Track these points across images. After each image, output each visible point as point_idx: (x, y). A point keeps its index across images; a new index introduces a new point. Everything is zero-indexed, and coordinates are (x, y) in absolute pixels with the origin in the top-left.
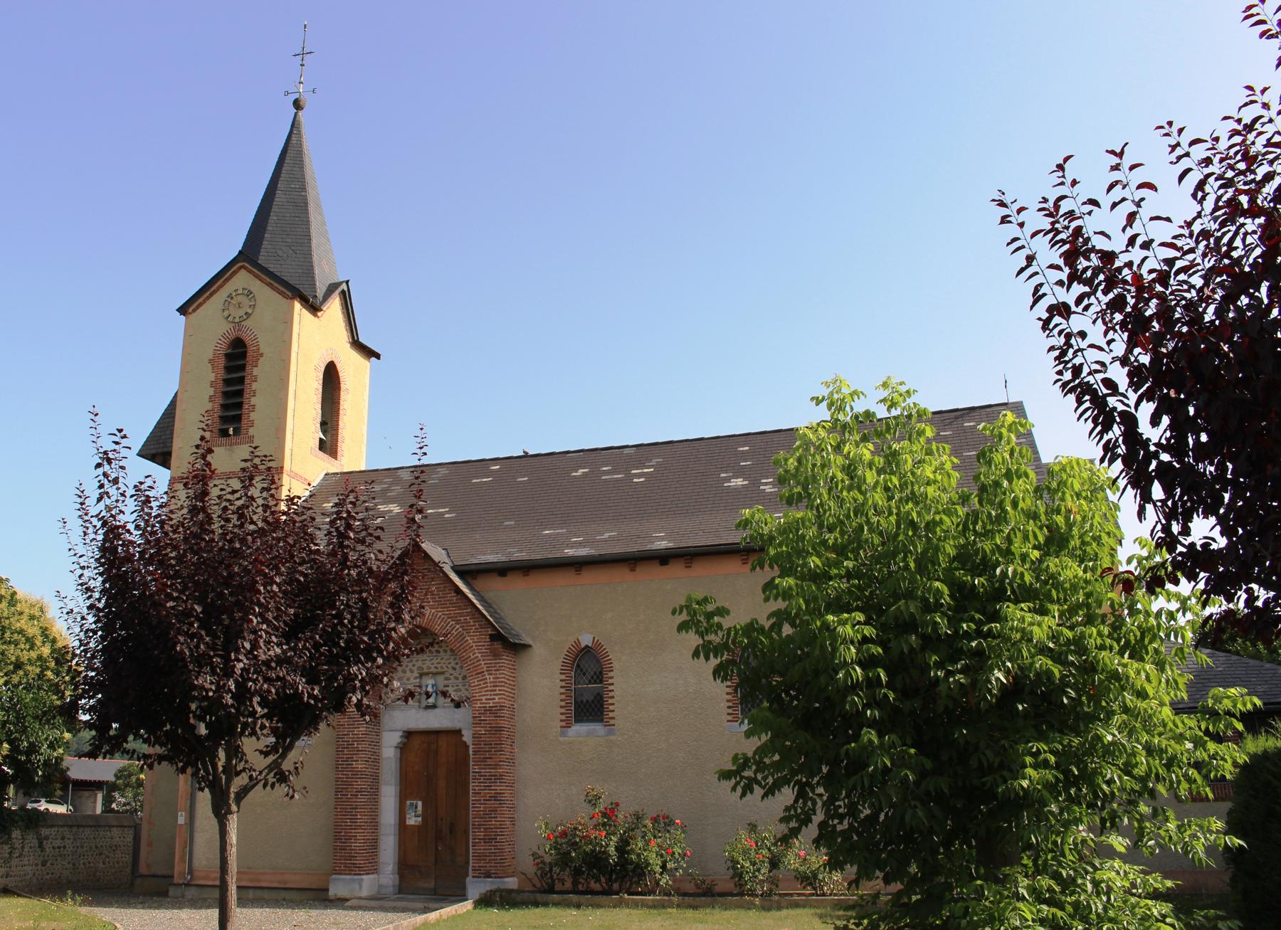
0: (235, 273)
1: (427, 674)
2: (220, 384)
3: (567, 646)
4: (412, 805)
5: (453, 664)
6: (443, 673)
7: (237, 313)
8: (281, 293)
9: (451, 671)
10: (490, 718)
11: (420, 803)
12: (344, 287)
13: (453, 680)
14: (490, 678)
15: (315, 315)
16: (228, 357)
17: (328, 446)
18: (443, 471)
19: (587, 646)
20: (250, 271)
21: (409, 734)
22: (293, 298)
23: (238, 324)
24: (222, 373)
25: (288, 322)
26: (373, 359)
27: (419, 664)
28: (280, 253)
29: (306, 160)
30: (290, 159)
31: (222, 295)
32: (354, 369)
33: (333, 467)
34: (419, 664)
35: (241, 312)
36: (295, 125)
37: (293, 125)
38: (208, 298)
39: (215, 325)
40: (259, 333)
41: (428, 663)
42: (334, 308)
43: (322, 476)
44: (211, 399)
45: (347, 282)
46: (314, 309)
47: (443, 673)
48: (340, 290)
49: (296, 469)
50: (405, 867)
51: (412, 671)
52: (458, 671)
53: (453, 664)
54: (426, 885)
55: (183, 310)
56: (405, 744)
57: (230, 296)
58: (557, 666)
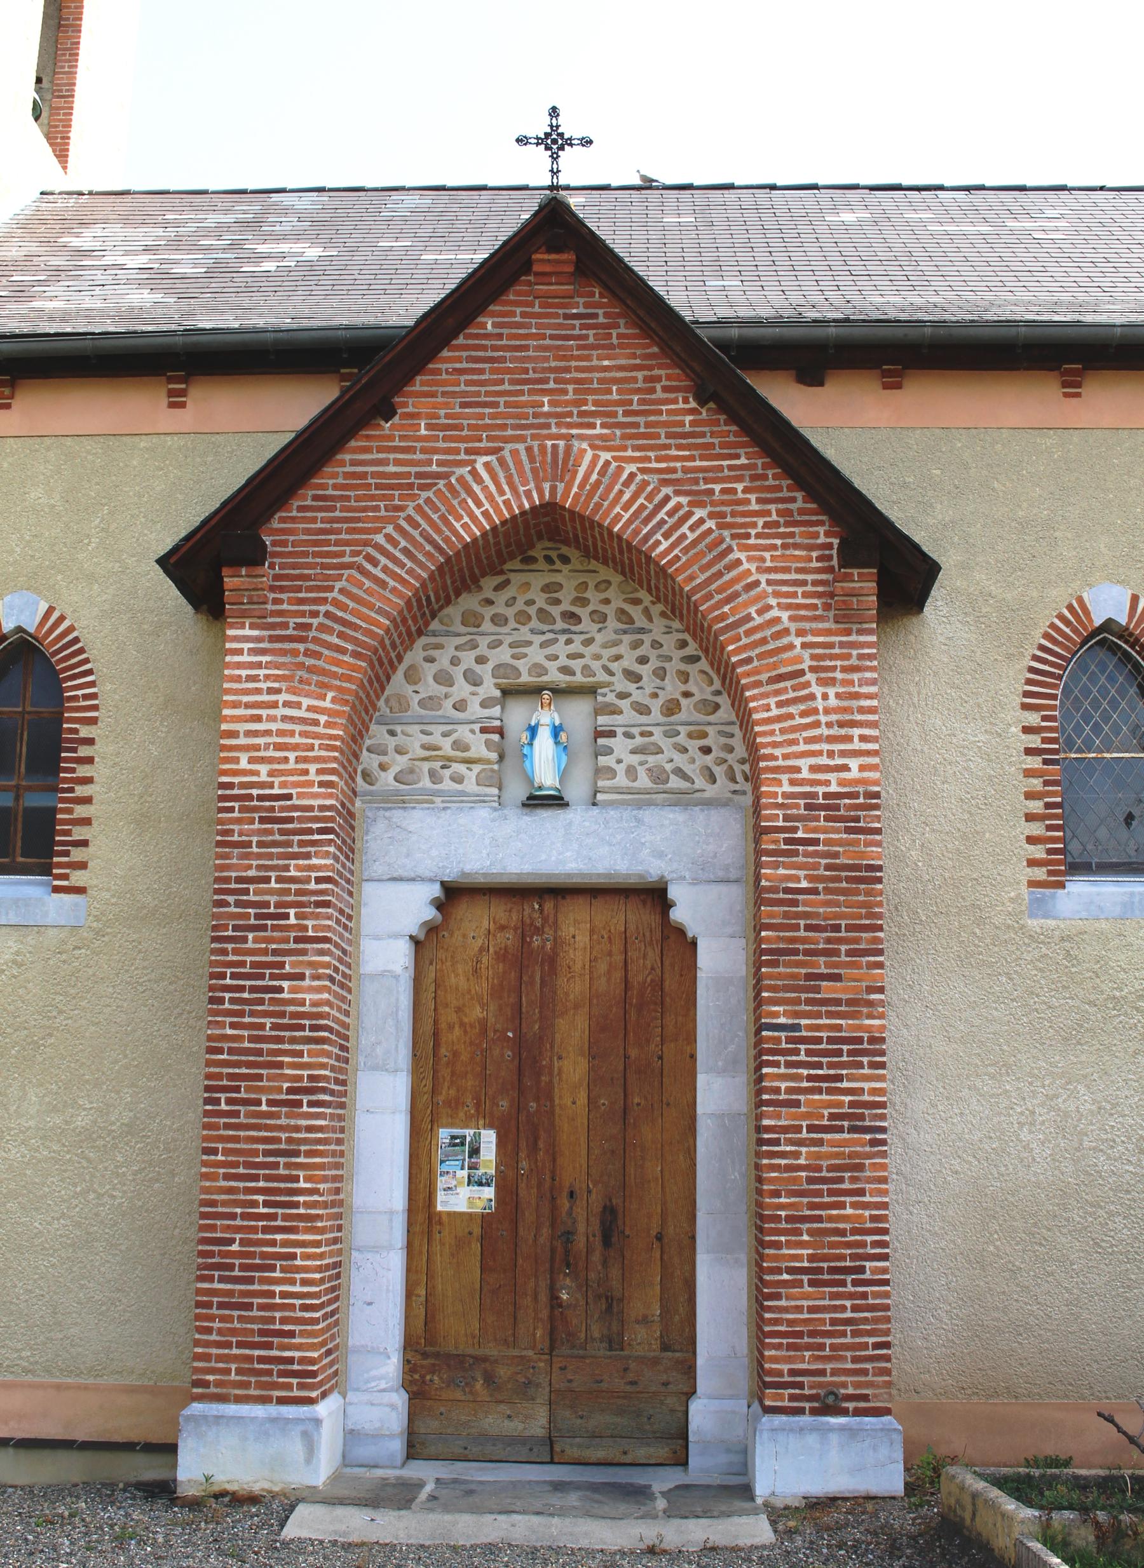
1: (534, 691)
3: (1045, 619)
4: (457, 1142)
5: (629, 661)
6: (590, 691)
9: (621, 684)
10: (829, 834)
11: (489, 1139)
13: (629, 716)
14: (825, 697)
18: (413, 200)
19: (1109, 625)
21: (454, 895)
27: (503, 655)
33: (58, 181)
34: (503, 655)
41: (535, 654)
47: (590, 691)
50: (429, 1363)
51: (474, 680)
52: (649, 683)
53: (629, 661)
54: (514, 1427)
56: (432, 929)
58: (1011, 681)
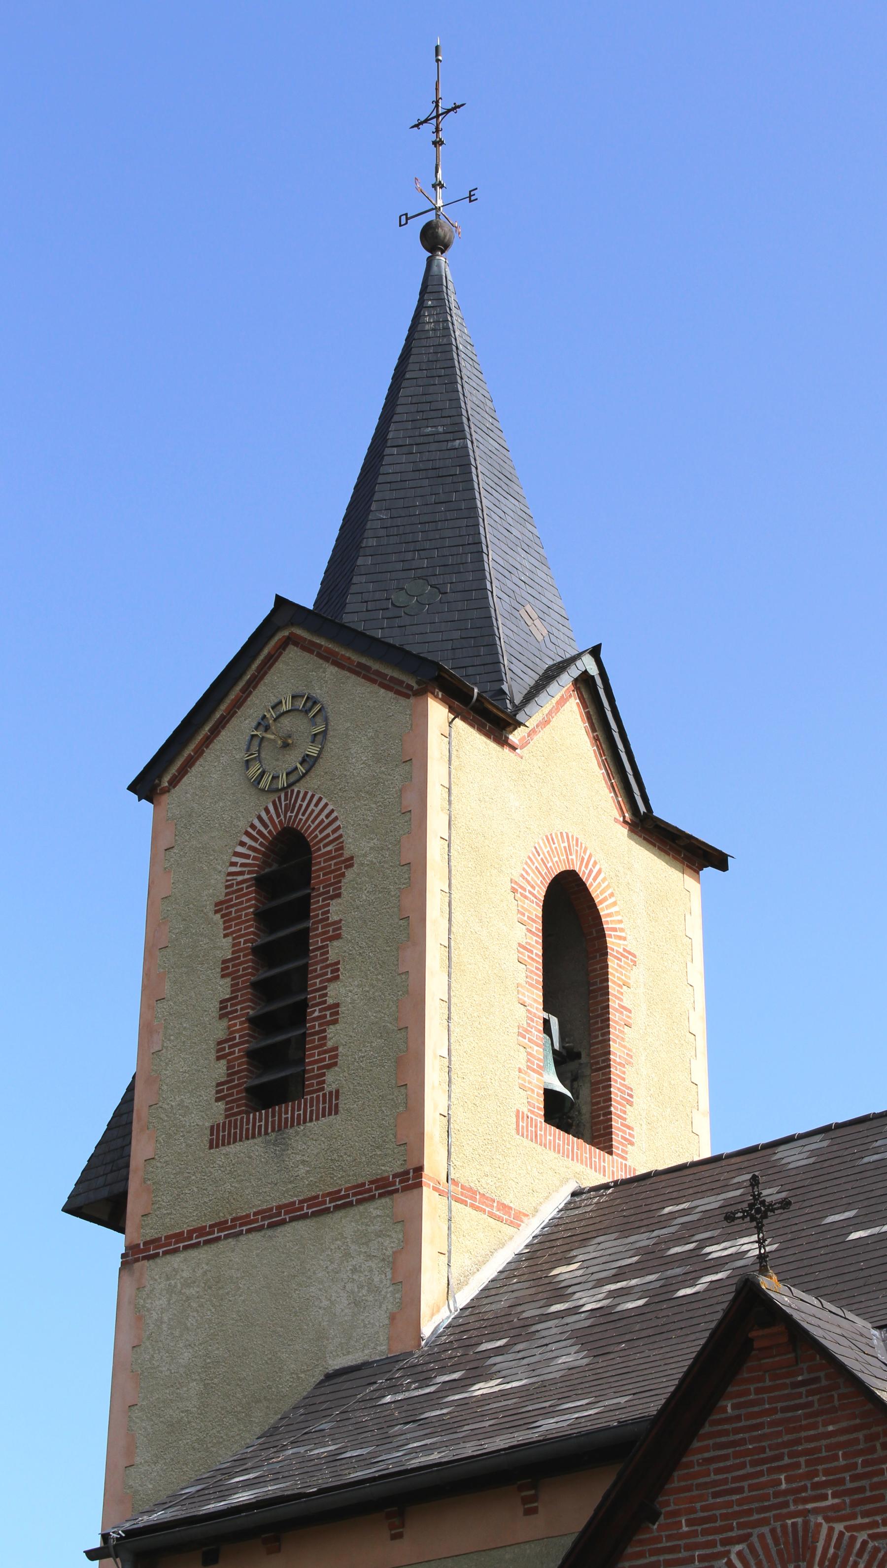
0: (271, 660)
2: (247, 961)
7: (281, 765)
8: (389, 685)
12: (589, 664)
15: (502, 741)
16: (265, 884)
17: (579, 1104)
20: (308, 648)
22: (421, 693)
23: (284, 792)
24: (249, 929)
25: (413, 762)
26: (709, 872)
28: (400, 598)
29: (466, 368)
30: (425, 386)
31: (243, 725)
32: (636, 891)
35: (293, 759)
36: (431, 288)
37: (423, 291)
38: (208, 741)
39: (226, 800)
40: (340, 810)
42: (559, 726)
43: (562, 1197)
44: (225, 1010)
45: (595, 652)
46: (495, 719)
48: (575, 671)
49: (465, 1174)
55: (146, 785)
57: (263, 724)
